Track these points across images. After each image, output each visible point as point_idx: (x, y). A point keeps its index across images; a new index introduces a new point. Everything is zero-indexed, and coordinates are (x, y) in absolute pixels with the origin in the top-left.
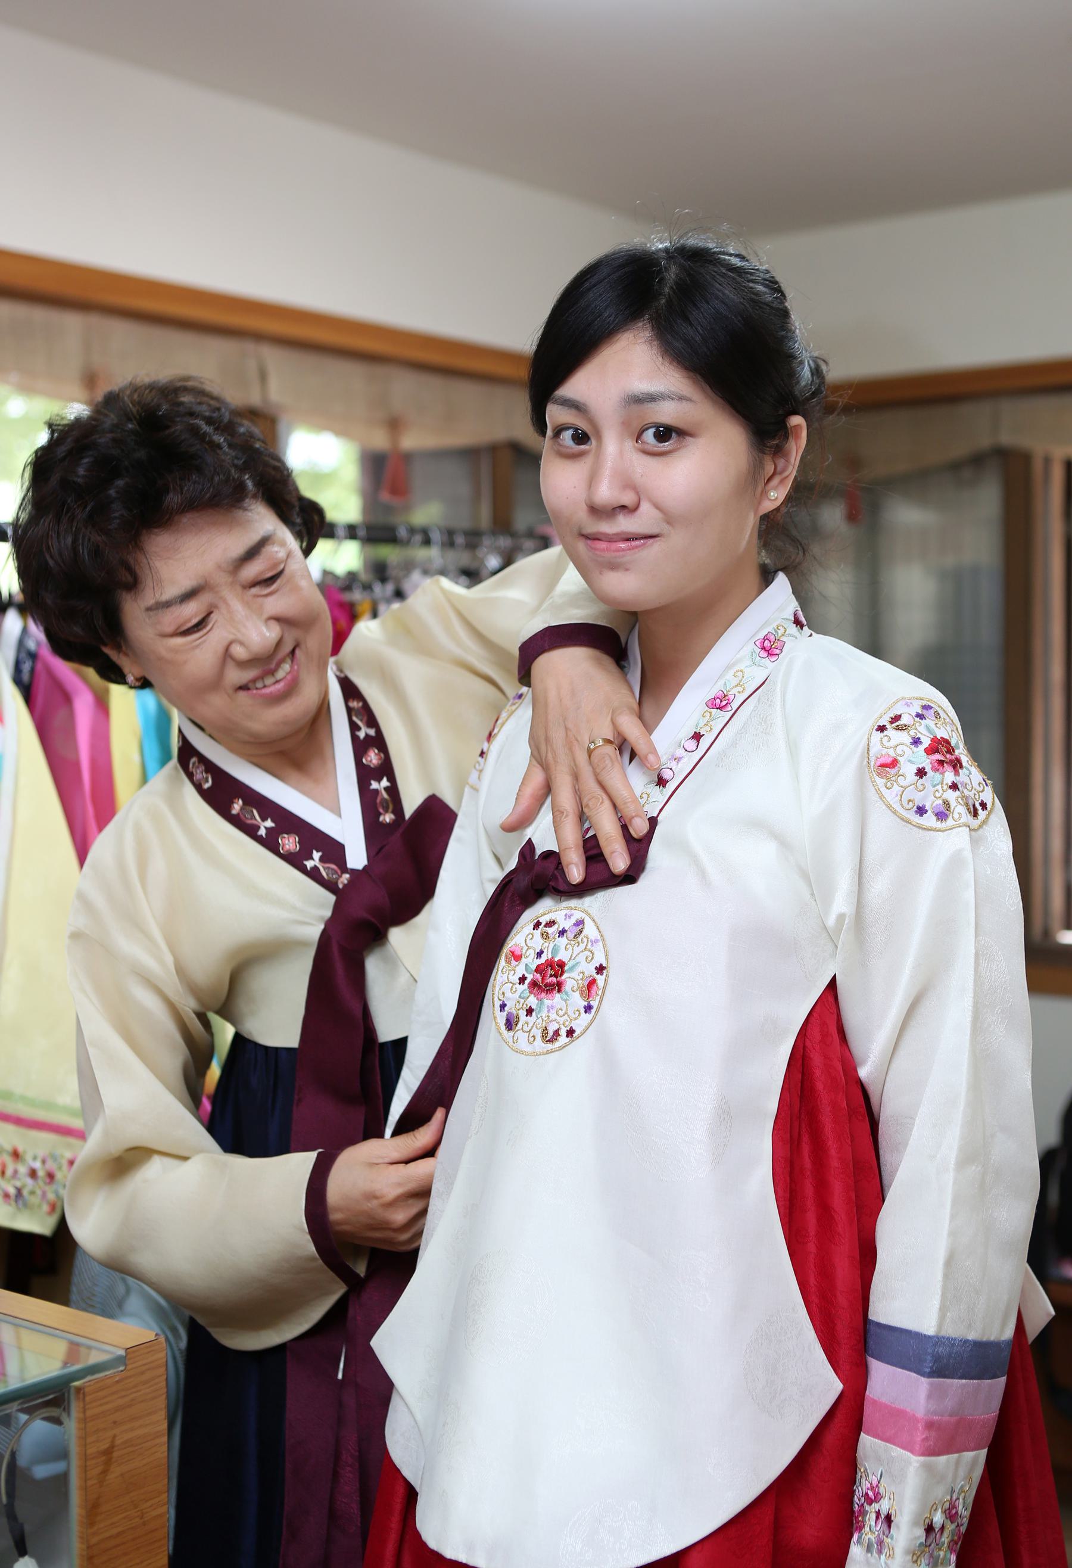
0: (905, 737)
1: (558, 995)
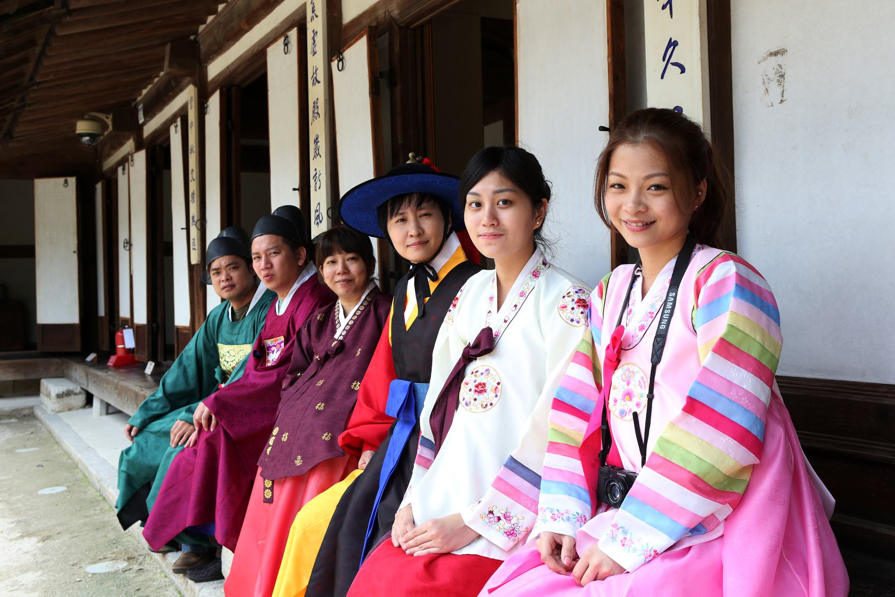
0: (570, 299)
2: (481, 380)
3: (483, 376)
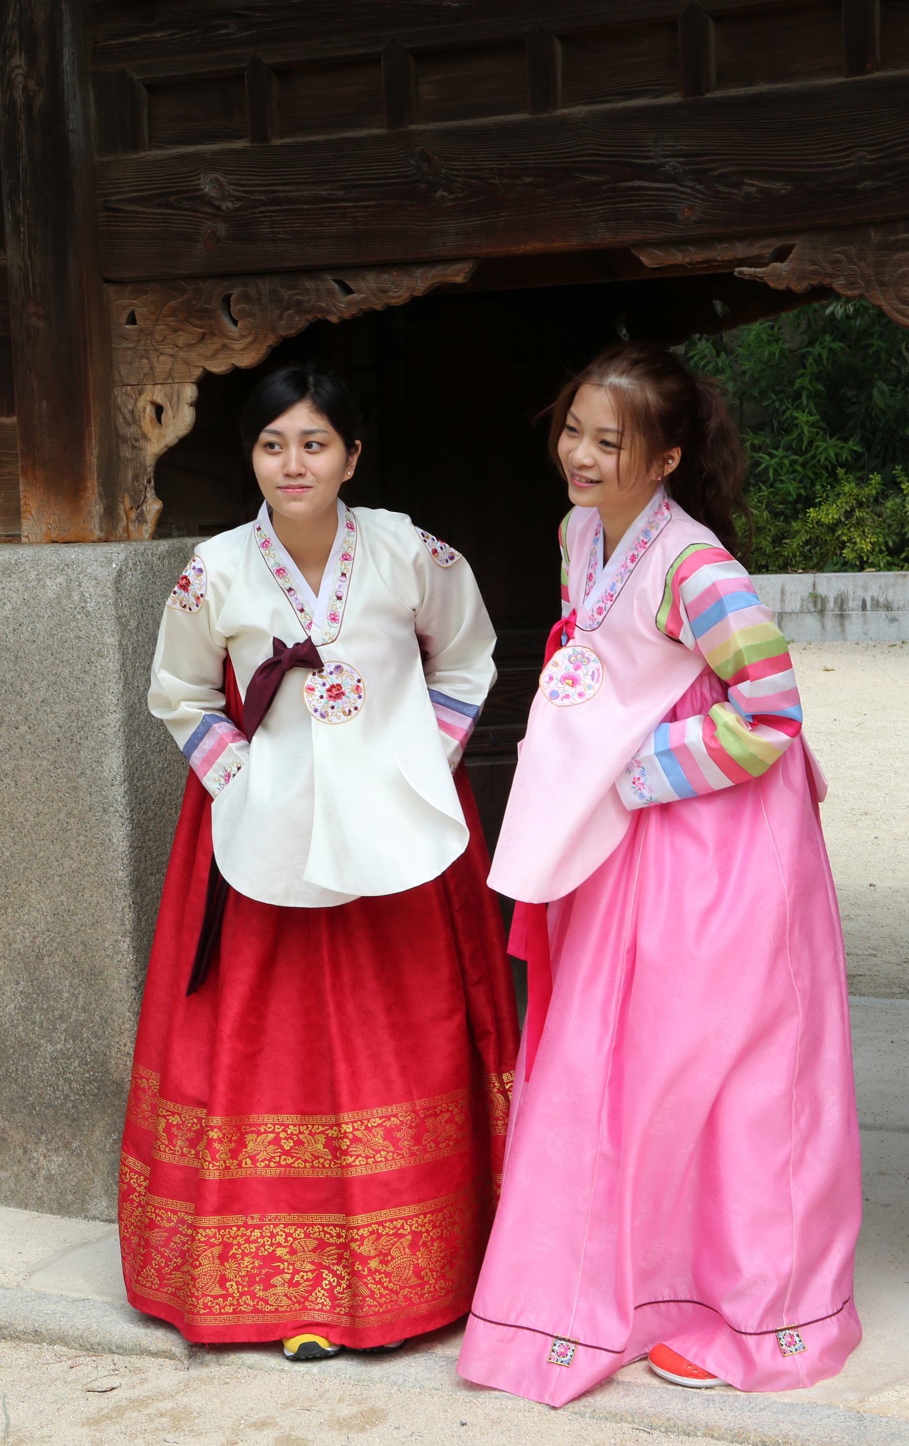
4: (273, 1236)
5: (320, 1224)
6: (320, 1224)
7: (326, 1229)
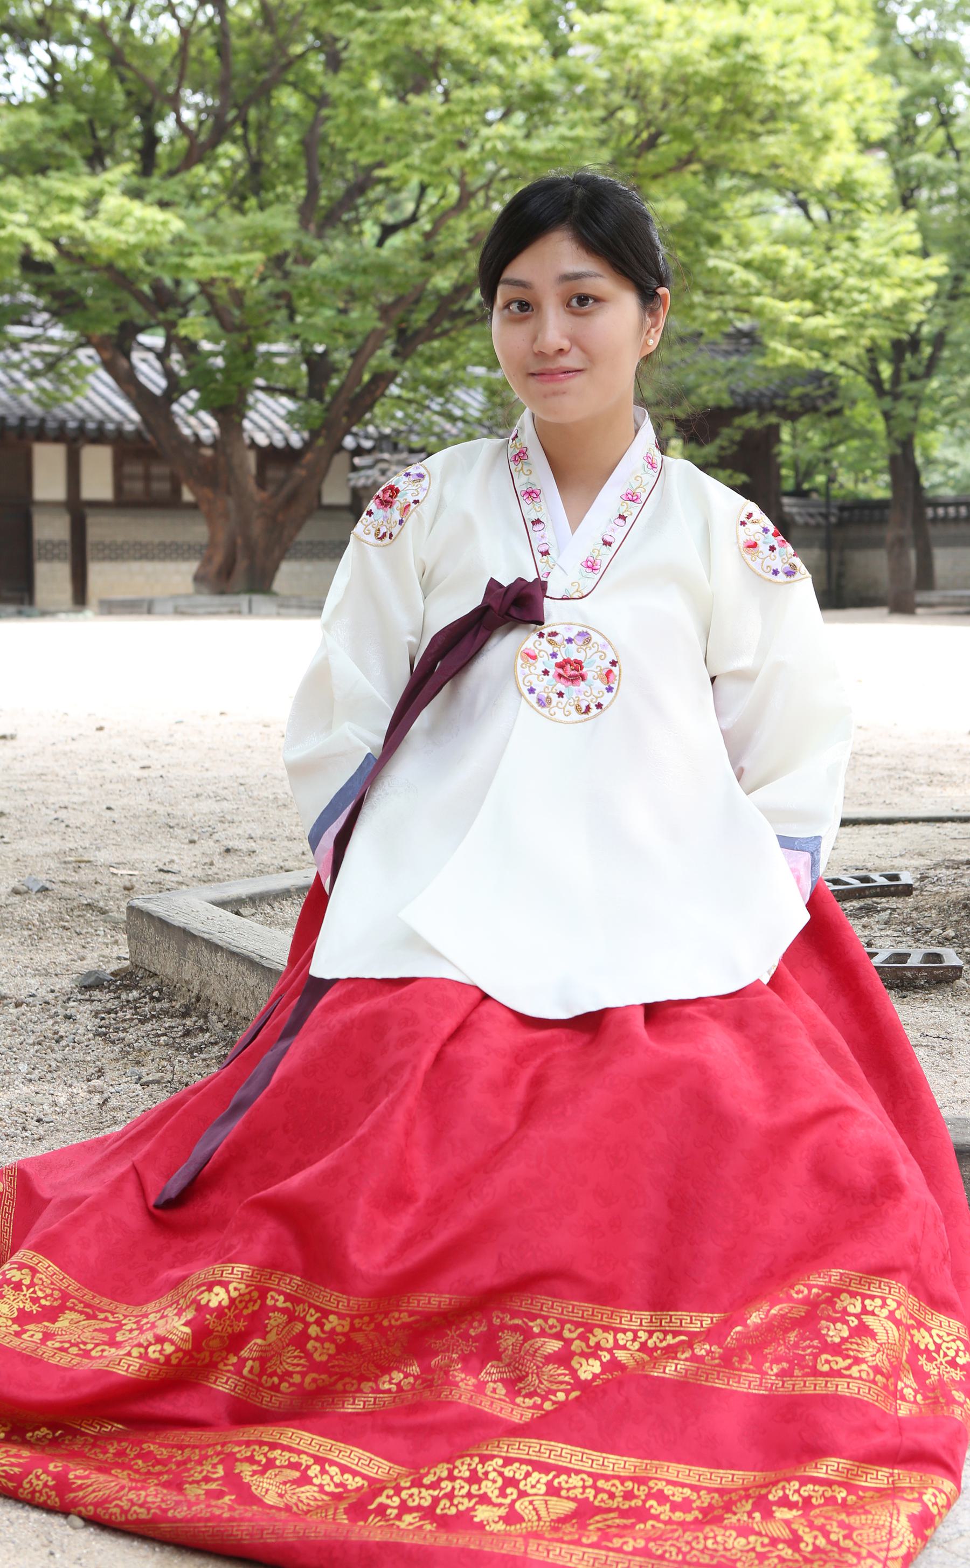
0: (550, 649)
1: (582, 683)
2: (573, 652)
3: (573, 646)
4: (474, 1478)
5: (590, 1474)
6: (590, 1474)
7: (601, 1483)
